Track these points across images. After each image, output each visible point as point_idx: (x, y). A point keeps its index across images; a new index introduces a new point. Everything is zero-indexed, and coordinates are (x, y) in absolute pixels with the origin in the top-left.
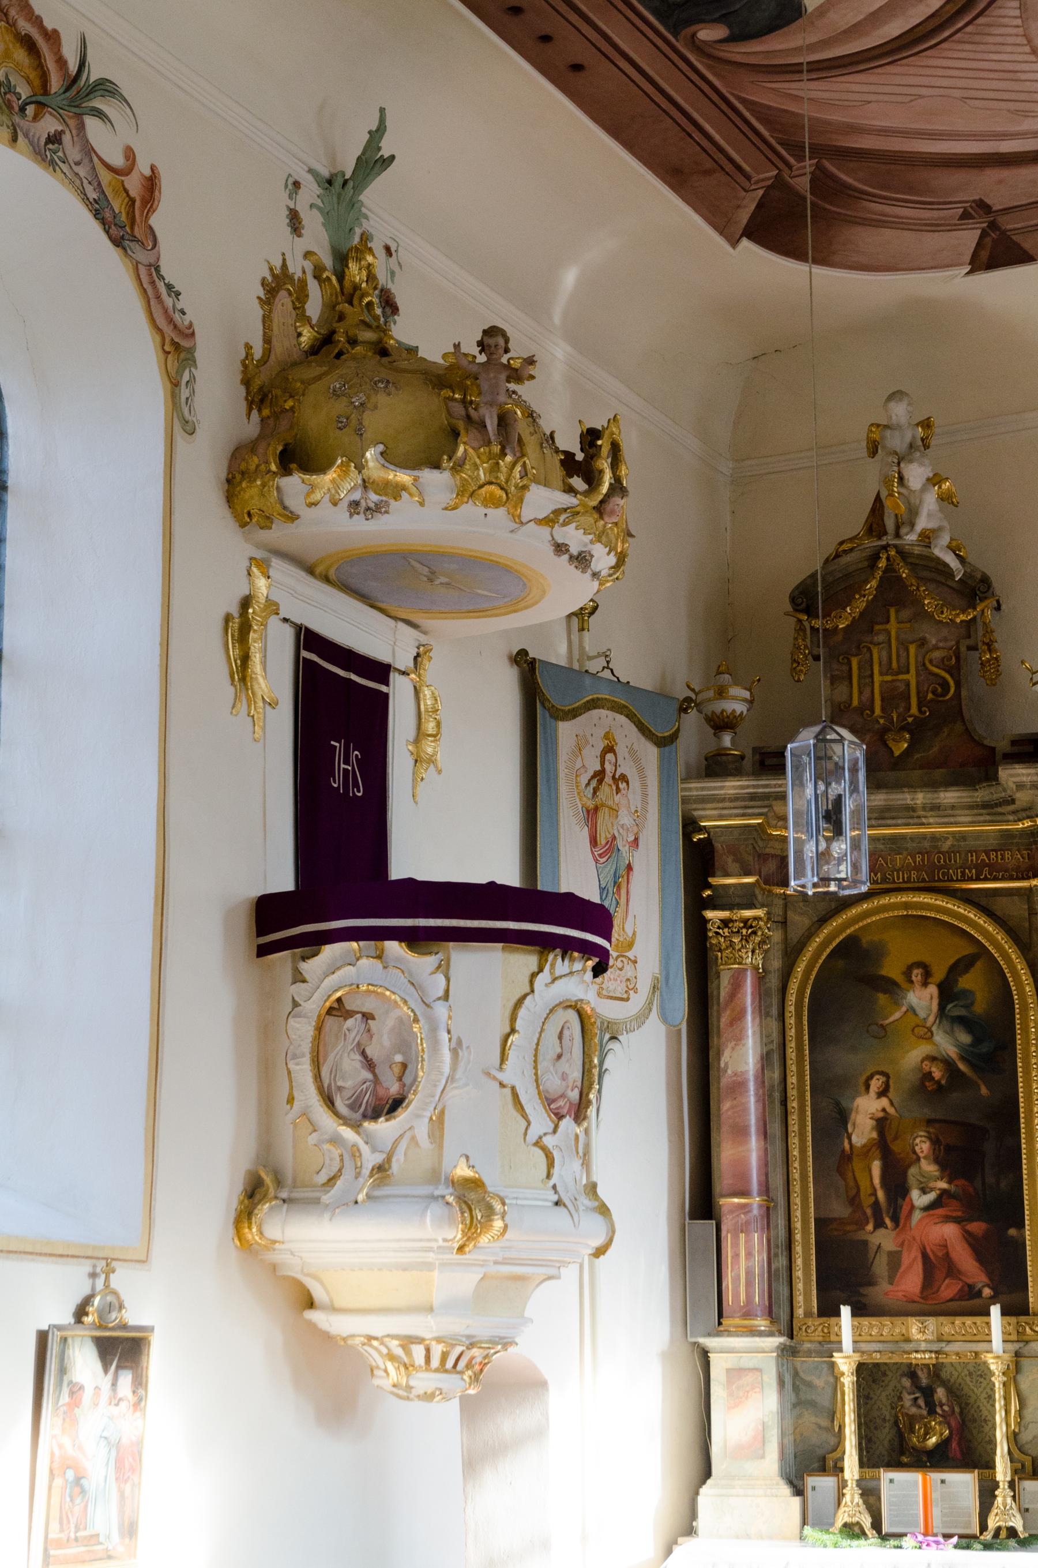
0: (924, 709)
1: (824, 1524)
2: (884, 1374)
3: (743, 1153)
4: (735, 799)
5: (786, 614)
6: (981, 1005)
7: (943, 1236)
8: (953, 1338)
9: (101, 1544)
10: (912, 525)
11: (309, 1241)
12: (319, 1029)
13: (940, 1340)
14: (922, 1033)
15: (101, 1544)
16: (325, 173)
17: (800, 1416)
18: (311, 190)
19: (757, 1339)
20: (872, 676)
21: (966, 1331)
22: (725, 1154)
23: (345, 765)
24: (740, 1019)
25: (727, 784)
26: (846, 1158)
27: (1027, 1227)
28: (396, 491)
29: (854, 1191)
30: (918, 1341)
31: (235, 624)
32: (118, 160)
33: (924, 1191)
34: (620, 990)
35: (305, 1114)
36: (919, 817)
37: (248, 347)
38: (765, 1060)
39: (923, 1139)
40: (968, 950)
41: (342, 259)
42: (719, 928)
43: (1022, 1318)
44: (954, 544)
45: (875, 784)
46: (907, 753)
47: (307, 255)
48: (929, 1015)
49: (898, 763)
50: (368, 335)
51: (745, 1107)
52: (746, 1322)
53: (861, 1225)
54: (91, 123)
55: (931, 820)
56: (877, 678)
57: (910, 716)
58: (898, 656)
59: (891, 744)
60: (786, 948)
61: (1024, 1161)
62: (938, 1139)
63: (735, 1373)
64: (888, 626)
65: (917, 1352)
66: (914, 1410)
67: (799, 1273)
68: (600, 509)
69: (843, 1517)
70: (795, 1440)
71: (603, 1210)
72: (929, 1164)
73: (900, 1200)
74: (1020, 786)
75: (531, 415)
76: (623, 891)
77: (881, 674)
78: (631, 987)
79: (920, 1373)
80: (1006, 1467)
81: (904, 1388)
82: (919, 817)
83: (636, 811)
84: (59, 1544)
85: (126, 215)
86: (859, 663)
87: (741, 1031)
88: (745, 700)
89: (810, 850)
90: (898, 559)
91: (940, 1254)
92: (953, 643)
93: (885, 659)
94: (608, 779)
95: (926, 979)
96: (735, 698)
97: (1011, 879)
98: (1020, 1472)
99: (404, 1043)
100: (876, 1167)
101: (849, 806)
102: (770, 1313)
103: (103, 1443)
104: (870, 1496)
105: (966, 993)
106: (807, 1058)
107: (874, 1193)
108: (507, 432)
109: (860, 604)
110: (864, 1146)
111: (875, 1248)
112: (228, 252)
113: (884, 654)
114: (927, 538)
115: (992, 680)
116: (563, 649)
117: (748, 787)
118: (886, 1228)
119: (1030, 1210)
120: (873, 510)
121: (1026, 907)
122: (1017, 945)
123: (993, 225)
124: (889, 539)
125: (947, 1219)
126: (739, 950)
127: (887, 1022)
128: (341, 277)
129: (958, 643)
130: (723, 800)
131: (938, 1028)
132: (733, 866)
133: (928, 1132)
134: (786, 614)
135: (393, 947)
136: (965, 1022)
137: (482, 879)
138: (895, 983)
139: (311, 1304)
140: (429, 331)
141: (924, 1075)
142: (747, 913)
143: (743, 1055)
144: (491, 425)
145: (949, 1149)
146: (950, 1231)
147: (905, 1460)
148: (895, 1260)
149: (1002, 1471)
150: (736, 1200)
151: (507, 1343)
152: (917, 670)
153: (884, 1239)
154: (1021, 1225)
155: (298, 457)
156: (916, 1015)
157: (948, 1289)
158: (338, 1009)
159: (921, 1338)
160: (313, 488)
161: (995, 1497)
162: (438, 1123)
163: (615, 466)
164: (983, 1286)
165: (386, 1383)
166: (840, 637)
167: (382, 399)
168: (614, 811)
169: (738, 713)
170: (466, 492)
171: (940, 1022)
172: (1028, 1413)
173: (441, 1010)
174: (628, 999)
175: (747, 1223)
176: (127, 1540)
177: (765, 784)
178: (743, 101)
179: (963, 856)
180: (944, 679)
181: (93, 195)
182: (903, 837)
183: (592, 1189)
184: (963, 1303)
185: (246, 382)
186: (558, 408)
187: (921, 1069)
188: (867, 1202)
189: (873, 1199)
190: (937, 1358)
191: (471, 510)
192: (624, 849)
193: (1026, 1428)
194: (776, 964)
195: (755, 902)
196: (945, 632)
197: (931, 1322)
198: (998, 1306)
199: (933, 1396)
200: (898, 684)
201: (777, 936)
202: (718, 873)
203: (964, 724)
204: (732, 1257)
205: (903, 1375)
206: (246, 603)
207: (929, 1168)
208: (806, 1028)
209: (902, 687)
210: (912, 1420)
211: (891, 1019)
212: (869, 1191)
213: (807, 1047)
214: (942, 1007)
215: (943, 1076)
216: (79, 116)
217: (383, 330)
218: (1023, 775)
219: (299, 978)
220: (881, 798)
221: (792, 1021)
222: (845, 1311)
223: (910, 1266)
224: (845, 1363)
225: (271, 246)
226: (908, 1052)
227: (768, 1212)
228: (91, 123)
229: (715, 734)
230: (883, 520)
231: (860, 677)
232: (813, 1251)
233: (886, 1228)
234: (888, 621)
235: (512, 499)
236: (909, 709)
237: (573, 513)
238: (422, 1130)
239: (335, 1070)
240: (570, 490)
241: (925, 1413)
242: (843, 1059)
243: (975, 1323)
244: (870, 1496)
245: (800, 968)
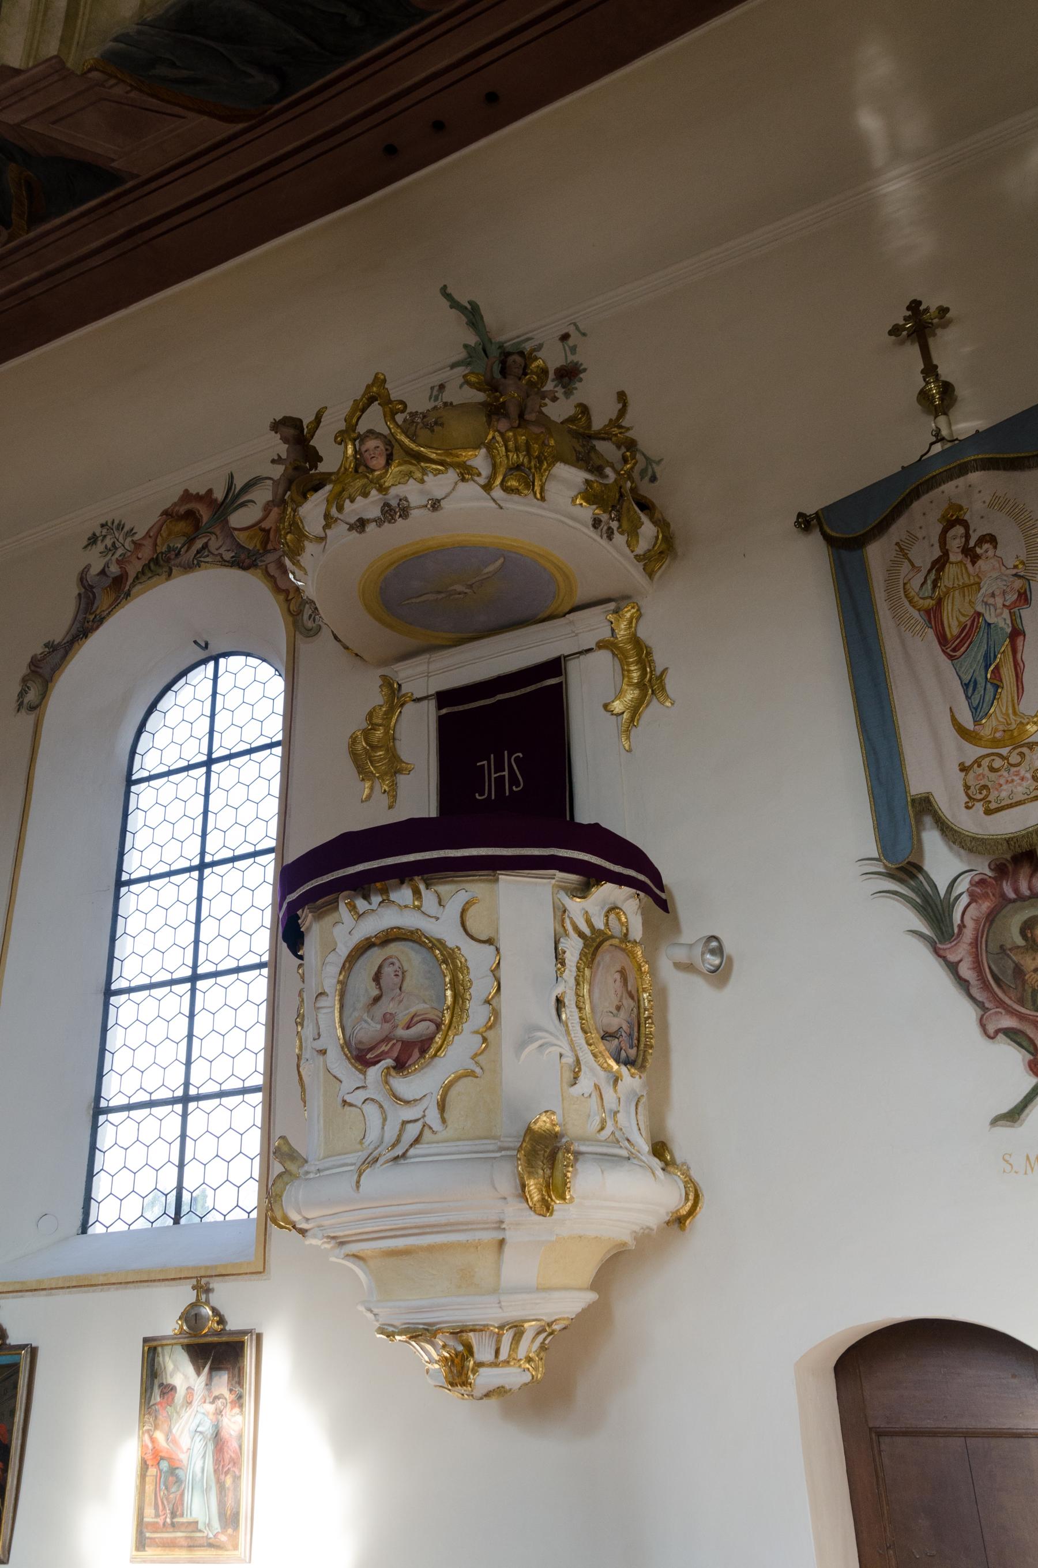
9: (200, 1531)
15: (200, 1531)
84: (154, 1527)
103: (198, 1437)
176: (230, 1531)
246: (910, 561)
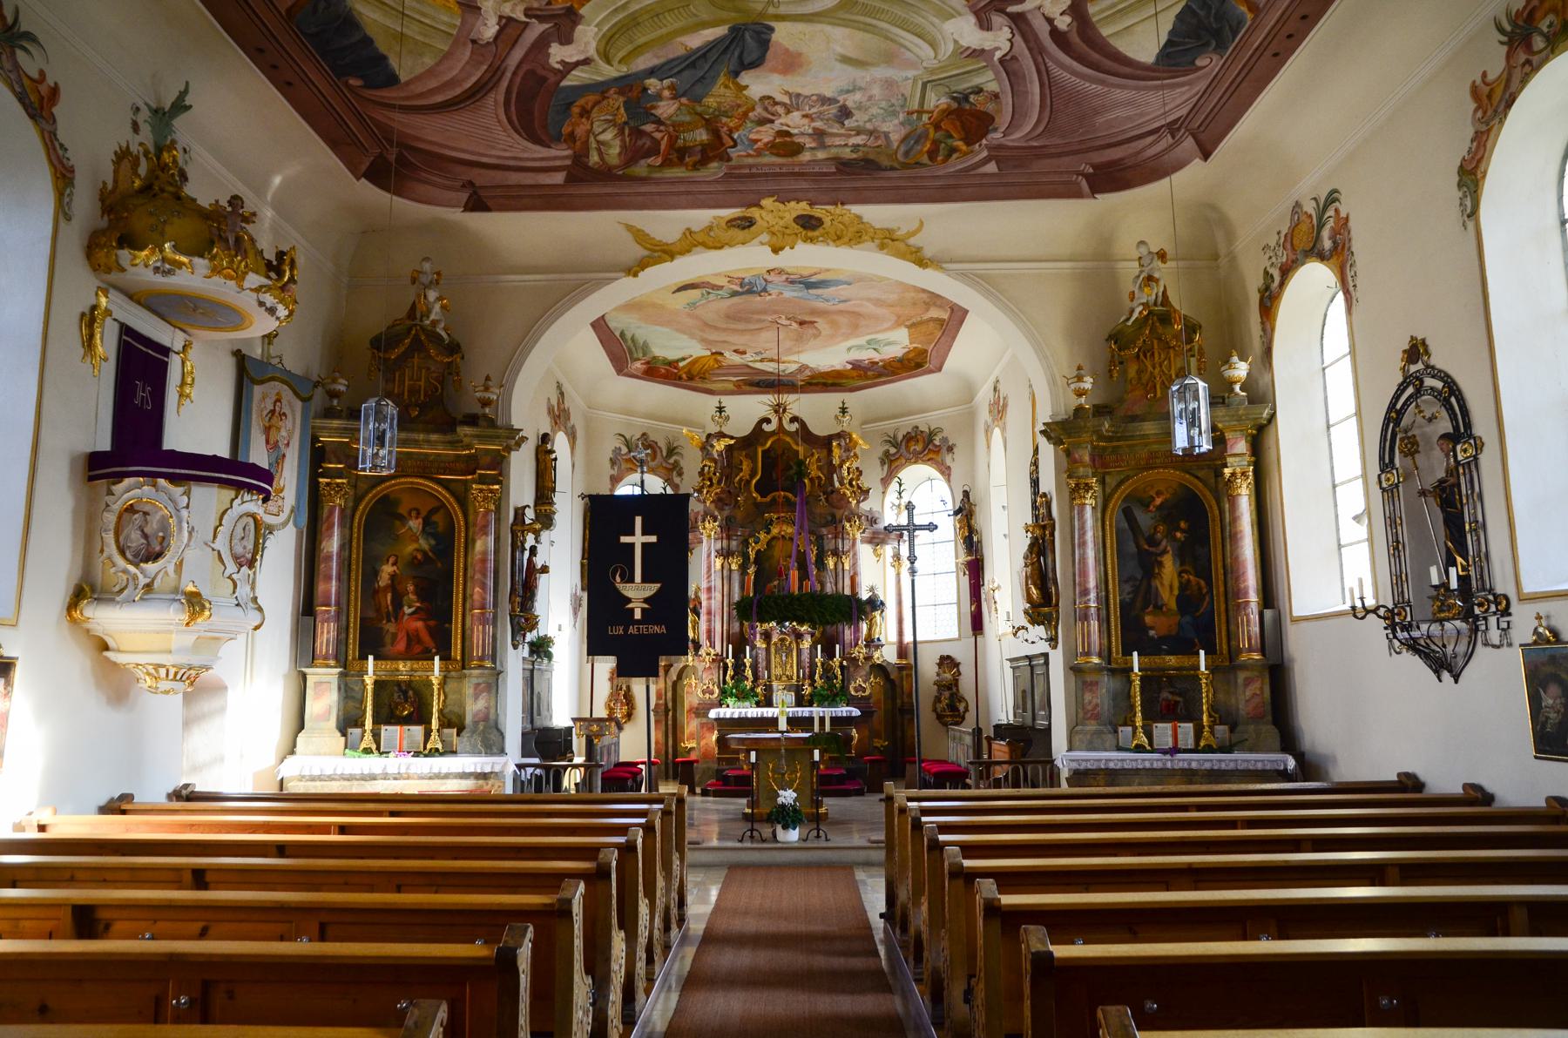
1: (354, 748)
6: (440, 529)
11: (104, 618)
12: (120, 517)
16: (154, 106)
18: (145, 114)
22: (321, 587)
23: (142, 393)
28: (180, 265)
31: (87, 318)
32: (35, 75)
34: (275, 511)
35: (109, 558)
37: (104, 183)
38: (342, 547)
40: (433, 504)
41: (159, 150)
45: (401, 428)
47: (141, 144)
49: (413, 421)
50: (171, 189)
54: (20, 54)
68: (283, 288)
69: (363, 745)
71: (260, 609)
75: (252, 240)
78: (280, 509)
85: (40, 104)
89: (369, 452)
98: (442, 725)
99: (164, 526)
101: (388, 435)
102: (336, 658)
104: (376, 736)
108: (241, 246)
109: (402, 349)
112: (98, 134)
114: (434, 323)
116: (259, 351)
123: (475, 193)
128: (158, 158)
135: (162, 481)
136: (434, 535)
137: (210, 453)
139: (106, 648)
140: (204, 190)
143: (333, 544)
144: (231, 241)
146: (419, 624)
148: (395, 636)
149: (435, 724)
151: (208, 668)
153: (391, 627)
155: (130, 241)
157: (417, 649)
158: (131, 509)
160: (135, 257)
162: (179, 566)
163: (292, 270)
165: (146, 686)
167: (176, 220)
168: (279, 429)
170: (216, 271)
173: (184, 513)
177: (351, 424)
178: (371, 118)
181: (18, 89)
183: (255, 599)
185: (102, 200)
186: (266, 236)
188: (384, 610)
191: (217, 279)
197: (409, 663)
201: (352, 492)
206: (94, 308)
207: (412, 597)
210: (397, 704)
216: (12, 48)
217: (180, 188)
219: (110, 493)
220: (403, 435)
222: (371, 658)
224: (369, 680)
225: (121, 135)
227: (338, 613)
228: (20, 54)
235: (240, 278)
237: (269, 289)
238: (171, 569)
239: (127, 537)
240: (269, 277)
244: (376, 736)
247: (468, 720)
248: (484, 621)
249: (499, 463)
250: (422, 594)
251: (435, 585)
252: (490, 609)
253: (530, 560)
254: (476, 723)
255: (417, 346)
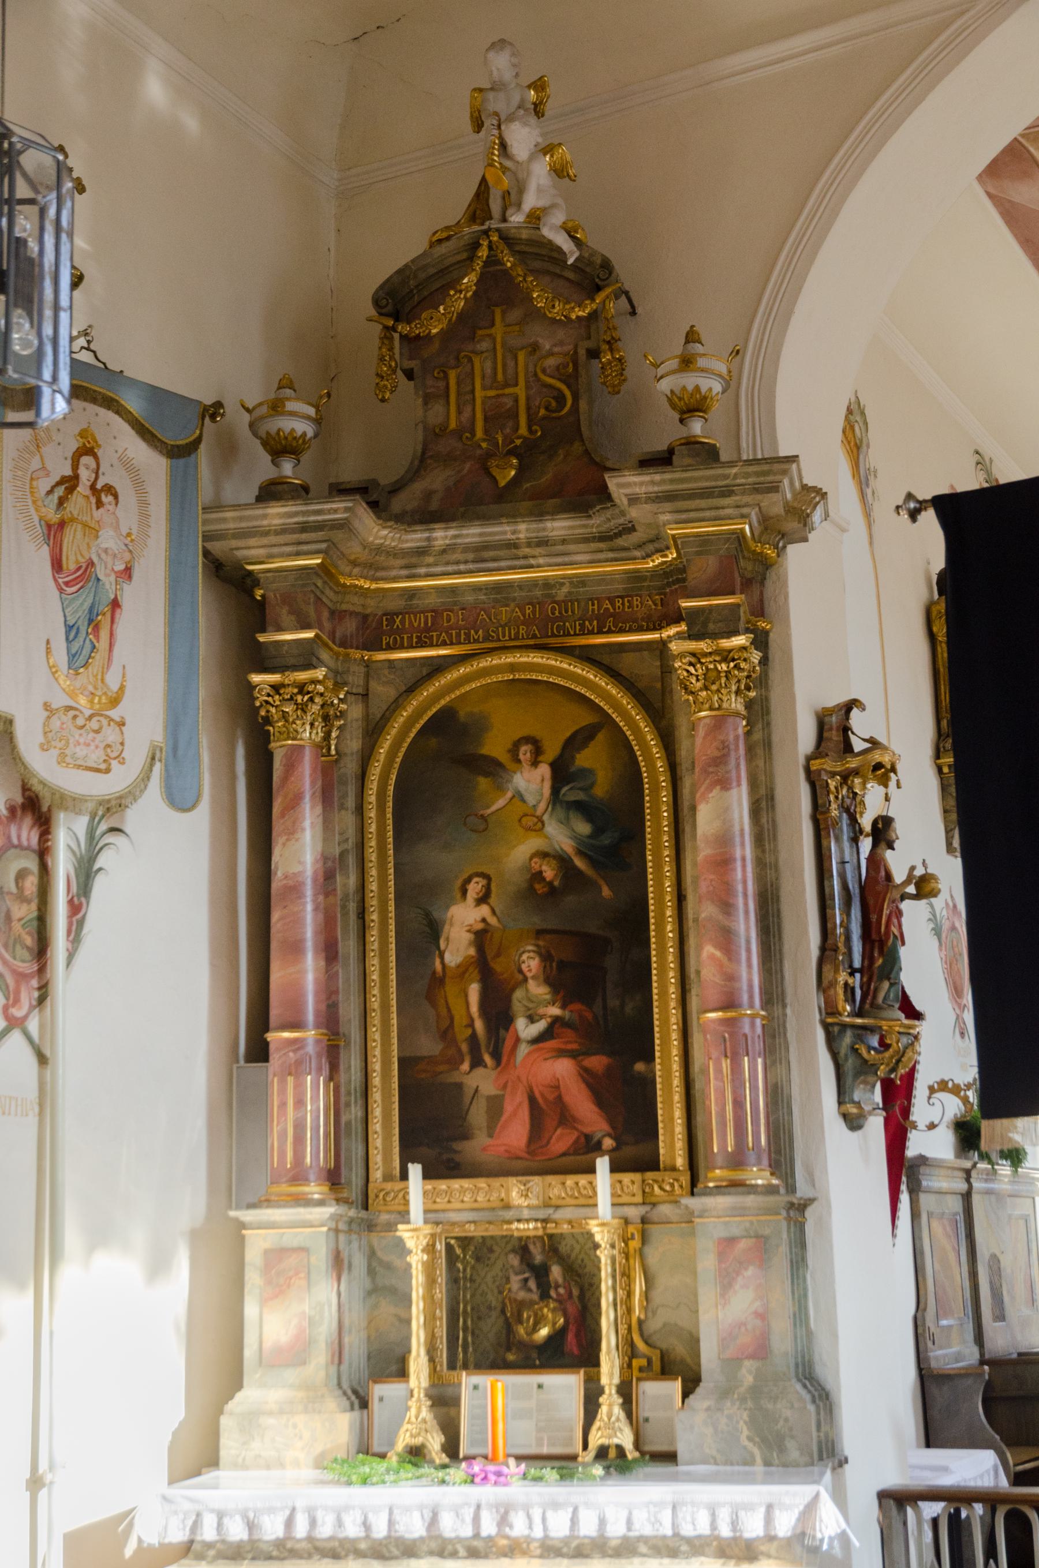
0: (535, 427)
2: (491, 1250)
3: (301, 976)
4: (283, 531)
5: (370, 320)
6: (602, 788)
7: (554, 1076)
8: (563, 1202)
10: (519, 205)
13: (547, 1206)
14: (530, 824)
17: (375, 1306)
19: (301, 1210)
20: (473, 391)
21: (579, 1192)
24: (293, 808)
25: (270, 511)
26: (438, 981)
27: (658, 1061)
29: (447, 1023)
30: (519, 1207)
33: (532, 1019)
36: (525, 557)
39: (532, 954)
40: (587, 719)
42: (269, 695)
43: (650, 1175)
44: (570, 224)
46: (515, 482)
48: (539, 802)
51: (303, 918)
52: (294, 1189)
53: (454, 1063)
55: (541, 561)
56: (479, 394)
57: (518, 438)
58: (504, 366)
59: (495, 472)
60: (367, 725)
61: (654, 978)
62: (548, 952)
63: (275, 1256)
64: (492, 331)
65: (519, 1221)
66: (522, 1295)
67: (376, 1126)
70: (369, 1337)
72: (539, 986)
73: (502, 1032)
74: (633, 500)
76: (104, 634)
77: (484, 388)
79: (531, 1247)
80: (612, 1367)
81: (512, 1267)
82: (525, 557)
83: (129, 535)
86: (458, 377)
87: (294, 823)
88: (308, 418)
90: (502, 245)
91: (551, 1097)
92: (571, 347)
93: (489, 371)
94: (83, 488)
95: (536, 758)
96: (293, 414)
97: (640, 630)
100: (474, 991)
102: (333, 1178)
105: (586, 773)
106: (391, 859)
107: (471, 1025)
110: (458, 966)
111: (472, 1092)
113: (488, 364)
114: (535, 218)
115: (614, 386)
117: (296, 514)
118: (486, 1066)
119: (660, 1038)
120: (477, 195)
121: (658, 663)
122: (646, 712)
124: (494, 224)
125: (561, 1053)
126: (294, 722)
127: (489, 811)
129: (576, 347)
130: (267, 534)
131: (551, 815)
132: (286, 618)
133: (537, 946)
134: (370, 320)
136: (583, 809)
138: (499, 764)
141: (533, 874)
142: (303, 676)
145: (562, 965)
146: (563, 1068)
147: (511, 1357)
148: (495, 1107)
150: (286, 1035)
152: (527, 382)
153: (482, 1081)
154: (650, 1058)
156: (523, 800)
157: (561, 1141)
159: (522, 1204)
161: (599, 1406)
164: (604, 1136)
166: (437, 345)
168: (93, 531)
169: (299, 433)
171: (553, 809)
172: (657, 1296)
174: (108, 771)
175: (299, 1063)
179: (583, 604)
180: (559, 390)
182: (508, 585)
184: (579, 1158)
187: (529, 868)
188: (462, 1034)
189: (469, 1031)
190: (544, 1228)
192: (108, 581)
193: (654, 1313)
194: (354, 745)
195: (314, 661)
196: (561, 334)
197: (536, 1182)
198: (606, 1158)
199: (547, 1275)
200: (505, 400)
202: (270, 628)
203: (584, 444)
204: (279, 1107)
205: (513, 1251)
207: (538, 990)
208: (390, 822)
209: (509, 403)
210: (521, 1305)
211: (494, 808)
212: (465, 1022)
213: (391, 846)
214: (555, 791)
215: (556, 875)
218: (635, 484)
221: (373, 814)
223: (515, 1113)
226: (515, 846)
229: (273, 461)
230: (488, 205)
231: (459, 394)
232: (396, 1099)
233: (486, 1066)
234: (493, 325)
236: (517, 429)
241: (535, 1297)
242: (435, 858)
243: (620, 1182)
244: (444, 1403)
245: (383, 751)
246: (41, 457)
247: (709, 1357)
248: (734, 1048)
249: (748, 576)
250: (573, 979)
251: (602, 955)
252: (752, 1010)
253: (875, 861)
254: (731, 1365)
255: (498, 290)
